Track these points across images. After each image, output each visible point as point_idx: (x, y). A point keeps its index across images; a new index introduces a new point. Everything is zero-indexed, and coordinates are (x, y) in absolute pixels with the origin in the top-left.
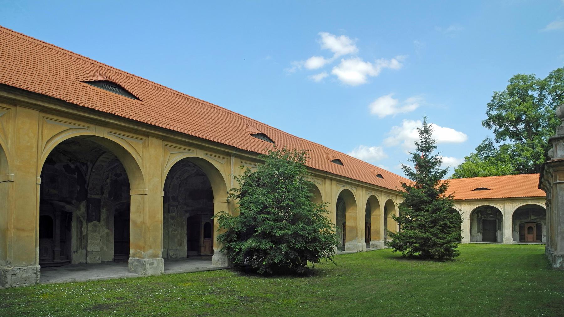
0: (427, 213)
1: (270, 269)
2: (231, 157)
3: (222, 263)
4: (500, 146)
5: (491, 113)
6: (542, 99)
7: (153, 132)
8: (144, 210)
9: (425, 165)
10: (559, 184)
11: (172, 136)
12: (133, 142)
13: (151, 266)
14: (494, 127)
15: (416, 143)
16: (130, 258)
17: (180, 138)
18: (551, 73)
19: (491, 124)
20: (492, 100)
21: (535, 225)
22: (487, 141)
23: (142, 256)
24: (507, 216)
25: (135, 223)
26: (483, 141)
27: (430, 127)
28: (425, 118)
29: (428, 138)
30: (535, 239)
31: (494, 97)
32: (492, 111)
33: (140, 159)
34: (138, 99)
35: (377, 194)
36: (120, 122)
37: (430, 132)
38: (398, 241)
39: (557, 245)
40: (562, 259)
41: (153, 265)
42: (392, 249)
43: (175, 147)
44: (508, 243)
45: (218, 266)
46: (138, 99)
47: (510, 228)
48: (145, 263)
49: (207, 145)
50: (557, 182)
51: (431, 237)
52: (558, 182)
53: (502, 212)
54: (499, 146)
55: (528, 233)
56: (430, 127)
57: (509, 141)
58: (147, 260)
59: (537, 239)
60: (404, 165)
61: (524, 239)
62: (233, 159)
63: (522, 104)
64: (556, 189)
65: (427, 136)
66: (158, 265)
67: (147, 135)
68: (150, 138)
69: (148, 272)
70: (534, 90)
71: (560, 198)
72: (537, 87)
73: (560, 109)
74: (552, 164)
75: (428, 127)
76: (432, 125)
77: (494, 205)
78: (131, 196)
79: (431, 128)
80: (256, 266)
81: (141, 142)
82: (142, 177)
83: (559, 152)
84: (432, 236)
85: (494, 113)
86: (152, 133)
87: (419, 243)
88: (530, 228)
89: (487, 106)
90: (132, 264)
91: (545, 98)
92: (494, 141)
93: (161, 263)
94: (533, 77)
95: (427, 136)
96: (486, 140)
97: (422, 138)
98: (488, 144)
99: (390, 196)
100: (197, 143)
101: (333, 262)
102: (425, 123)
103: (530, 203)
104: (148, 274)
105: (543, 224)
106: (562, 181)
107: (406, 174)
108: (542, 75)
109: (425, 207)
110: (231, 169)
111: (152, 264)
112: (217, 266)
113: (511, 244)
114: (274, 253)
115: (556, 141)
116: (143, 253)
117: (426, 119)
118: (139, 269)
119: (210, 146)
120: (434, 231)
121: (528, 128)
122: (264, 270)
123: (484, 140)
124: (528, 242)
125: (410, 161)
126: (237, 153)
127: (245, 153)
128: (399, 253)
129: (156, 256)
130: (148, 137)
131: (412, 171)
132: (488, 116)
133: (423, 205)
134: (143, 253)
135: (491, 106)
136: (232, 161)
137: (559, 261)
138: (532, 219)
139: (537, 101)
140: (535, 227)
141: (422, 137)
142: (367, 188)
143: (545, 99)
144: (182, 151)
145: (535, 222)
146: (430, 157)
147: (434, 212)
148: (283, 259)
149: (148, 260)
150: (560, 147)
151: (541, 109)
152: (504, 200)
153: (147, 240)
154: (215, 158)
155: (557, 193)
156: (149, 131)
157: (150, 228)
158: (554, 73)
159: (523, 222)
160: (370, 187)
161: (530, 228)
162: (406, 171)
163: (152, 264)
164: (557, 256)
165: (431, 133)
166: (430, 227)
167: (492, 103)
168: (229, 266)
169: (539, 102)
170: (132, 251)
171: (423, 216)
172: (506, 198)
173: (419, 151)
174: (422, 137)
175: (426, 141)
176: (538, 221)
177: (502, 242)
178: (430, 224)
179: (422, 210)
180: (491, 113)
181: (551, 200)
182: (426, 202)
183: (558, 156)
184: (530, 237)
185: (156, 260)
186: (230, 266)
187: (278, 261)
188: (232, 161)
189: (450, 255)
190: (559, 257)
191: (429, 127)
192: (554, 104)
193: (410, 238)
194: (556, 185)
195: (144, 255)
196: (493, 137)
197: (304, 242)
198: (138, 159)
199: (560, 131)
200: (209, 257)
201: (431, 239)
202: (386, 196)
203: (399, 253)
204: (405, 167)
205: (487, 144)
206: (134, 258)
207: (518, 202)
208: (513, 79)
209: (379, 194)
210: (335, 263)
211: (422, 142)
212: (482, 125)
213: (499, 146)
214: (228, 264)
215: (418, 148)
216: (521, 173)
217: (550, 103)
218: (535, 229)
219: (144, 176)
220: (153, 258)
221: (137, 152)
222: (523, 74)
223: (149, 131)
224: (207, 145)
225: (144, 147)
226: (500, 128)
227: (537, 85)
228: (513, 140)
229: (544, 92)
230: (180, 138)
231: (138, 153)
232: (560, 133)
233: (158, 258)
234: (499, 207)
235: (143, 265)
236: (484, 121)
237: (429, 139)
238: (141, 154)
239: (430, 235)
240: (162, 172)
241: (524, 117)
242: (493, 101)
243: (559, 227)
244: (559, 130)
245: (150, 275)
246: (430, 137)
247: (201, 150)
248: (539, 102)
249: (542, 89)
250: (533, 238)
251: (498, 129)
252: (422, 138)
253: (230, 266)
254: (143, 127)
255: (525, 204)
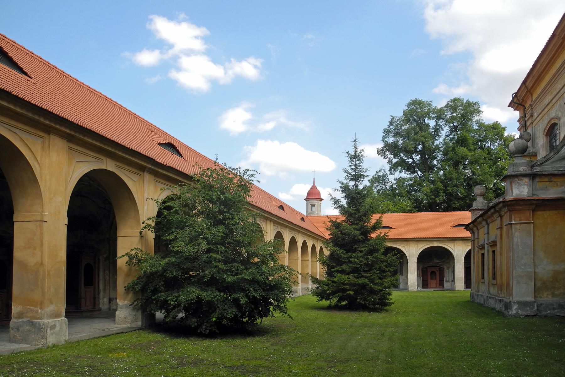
0: (360, 254)
1: (216, 327)
2: (145, 173)
3: (132, 322)
4: (395, 179)
5: (387, 140)
6: (437, 129)
7: (58, 127)
8: (42, 245)
9: (357, 197)
10: (515, 225)
11: (81, 137)
12: (28, 139)
13: (52, 331)
14: (389, 156)
15: (346, 172)
16: (13, 320)
17: (90, 140)
18: (449, 102)
19: (387, 153)
20: (388, 126)
21: (438, 270)
22: (381, 172)
23: (38, 316)
24: (412, 259)
25: (24, 265)
26: (377, 172)
27: (362, 151)
28: (356, 140)
29: (359, 164)
30: (438, 285)
31: (391, 123)
32: (387, 138)
33: (37, 166)
34: (25, 74)
35: (283, 230)
36: (15, 105)
37: (361, 158)
38: (326, 288)
39: (512, 290)
40: (517, 306)
41: (54, 328)
42: (315, 299)
43: (86, 155)
44: (413, 289)
45: (126, 326)
46: (25, 74)
47: (414, 273)
48: (44, 327)
49: (120, 153)
50: (513, 222)
51: (368, 283)
52: (513, 222)
53: (407, 255)
54: (394, 179)
55: (431, 279)
56: (362, 151)
57: (405, 175)
58: (46, 321)
59: (440, 285)
60: (332, 196)
61: (427, 285)
62: (147, 176)
63: (420, 134)
64: (512, 230)
65: (357, 162)
66: (61, 328)
67: (48, 130)
68: (52, 137)
69: (48, 341)
70: (430, 118)
71: (515, 240)
72: (433, 116)
73: (514, 145)
74: (509, 203)
75: (360, 152)
76: (364, 150)
77: (398, 246)
78: (15, 223)
79: (362, 153)
80: (196, 324)
81: (39, 141)
82: (39, 195)
83: (514, 190)
84: (369, 281)
85: (391, 140)
86: (56, 129)
87: (353, 290)
88: (433, 273)
89: (383, 132)
90: (18, 329)
91: (441, 128)
92: (388, 173)
93: (64, 325)
94: (429, 104)
95: (357, 162)
96: (380, 171)
97: (352, 164)
98: (381, 176)
99: (294, 232)
100: (110, 149)
101: (288, 315)
102: (355, 147)
103: (436, 244)
104: (48, 343)
105: (445, 268)
106: (517, 221)
107: (335, 207)
108: (440, 104)
109: (358, 248)
110: (145, 189)
111: (53, 327)
112: (124, 326)
113: (416, 291)
114: (222, 305)
115: (511, 179)
116: (40, 311)
117: (356, 142)
118: (33, 336)
119: (124, 155)
120: (371, 276)
121: (424, 160)
122: (209, 328)
123: (378, 170)
124: (431, 288)
125: (336, 190)
126: (153, 168)
127: (161, 169)
128: (325, 303)
129: (57, 315)
130: (49, 134)
131: (341, 203)
132: (383, 143)
133: (356, 245)
134: (40, 311)
135: (387, 132)
136: (146, 178)
137: (514, 308)
138: (435, 263)
139: (433, 130)
140: (438, 271)
141: (352, 163)
142: (275, 223)
143: (441, 129)
144: (89, 159)
145: (438, 266)
146: (361, 187)
147: (369, 254)
148: (237, 313)
149: (49, 322)
150: (515, 185)
151: (437, 140)
152: (409, 241)
153: (46, 290)
154: (127, 173)
155: (512, 234)
156: (53, 125)
157: (51, 273)
158: (451, 102)
159: (426, 266)
160: (278, 220)
161: (433, 273)
162: (335, 203)
163: (53, 327)
164: (512, 302)
165: (362, 159)
166: (365, 271)
167: (388, 129)
168: (142, 325)
169: (435, 132)
170: (15, 309)
171: (357, 257)
172: (411, 238)
173: (349, 180)
174: (352, 163)
175: (357, 168)
176: (441, 265)
177: (406, 290)
178: (365, 268)
179: (355, 251)
180: (387, 140)
181: (496, 241)
182: (359, 241)
183: (513, 194)
184: (433, 283)
185: (59, 320)
186: (144, 325)
187: (233, 316)
188: (146, 178)
189: (386, 305)
190: (514, 303)
191: (361, 152)
192: (451, 136)
193: (343, 284)
194: (511, 227)
195: (41, 314)
196: (387, 167)
197: (262, 290)
198: (35, 166)
199: (515, 167)
200: (110, 315)
201: (367, 285)
202: (290, 232)
203: (325, 303)
204: (335, 199)
205: (380, 176)
206: (21, 320)
207: (423, 243)
208: (410, 103)
209: (284, 230)
210: (290, 317)
211: (352, 169)
212: (377, 153)
213: (394, 179)
214: (142, 323)
215: (347, 176)
216: (419, 211)
217: (447, 134)
218: (438, 273)
219: (43, 194)
220: (54, 318)
221: (34, 155)
222: (420, 100)
223: (53, 125)
224: (120, 153)
225: (43, 148)
226: (394, 158)
227: (433, 114)
228: (407, 172)
229: (441, 122)
230: (90, 140)
231: (35, 158)
232: (515, 169)
233: (61, 317)
234: (449, 246)
235: (40, 330)
236: (379, 148)
237: (360, 166)
238: (39, 159)
239: (366, 281)
240: (66, 188)
241: (420, 147)
242: (390, 127)
243: (514, 271)
244: (513, 167)
245: (50, 344)
246: (361, 164)
247: (112, 159)
248: (435, 132)
249: (438, 118)
250: (436, 284)
251: (392, 159)
252: (352, 164)
253: (144, 325)
254: (45, 118)
255: (431, 245)
